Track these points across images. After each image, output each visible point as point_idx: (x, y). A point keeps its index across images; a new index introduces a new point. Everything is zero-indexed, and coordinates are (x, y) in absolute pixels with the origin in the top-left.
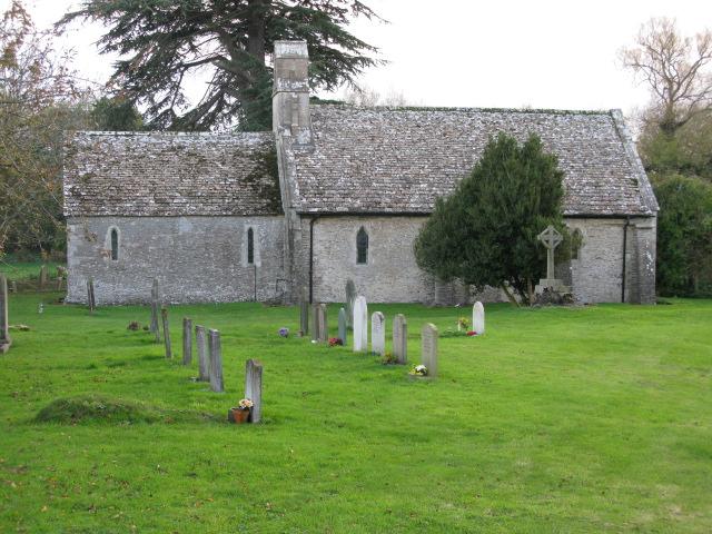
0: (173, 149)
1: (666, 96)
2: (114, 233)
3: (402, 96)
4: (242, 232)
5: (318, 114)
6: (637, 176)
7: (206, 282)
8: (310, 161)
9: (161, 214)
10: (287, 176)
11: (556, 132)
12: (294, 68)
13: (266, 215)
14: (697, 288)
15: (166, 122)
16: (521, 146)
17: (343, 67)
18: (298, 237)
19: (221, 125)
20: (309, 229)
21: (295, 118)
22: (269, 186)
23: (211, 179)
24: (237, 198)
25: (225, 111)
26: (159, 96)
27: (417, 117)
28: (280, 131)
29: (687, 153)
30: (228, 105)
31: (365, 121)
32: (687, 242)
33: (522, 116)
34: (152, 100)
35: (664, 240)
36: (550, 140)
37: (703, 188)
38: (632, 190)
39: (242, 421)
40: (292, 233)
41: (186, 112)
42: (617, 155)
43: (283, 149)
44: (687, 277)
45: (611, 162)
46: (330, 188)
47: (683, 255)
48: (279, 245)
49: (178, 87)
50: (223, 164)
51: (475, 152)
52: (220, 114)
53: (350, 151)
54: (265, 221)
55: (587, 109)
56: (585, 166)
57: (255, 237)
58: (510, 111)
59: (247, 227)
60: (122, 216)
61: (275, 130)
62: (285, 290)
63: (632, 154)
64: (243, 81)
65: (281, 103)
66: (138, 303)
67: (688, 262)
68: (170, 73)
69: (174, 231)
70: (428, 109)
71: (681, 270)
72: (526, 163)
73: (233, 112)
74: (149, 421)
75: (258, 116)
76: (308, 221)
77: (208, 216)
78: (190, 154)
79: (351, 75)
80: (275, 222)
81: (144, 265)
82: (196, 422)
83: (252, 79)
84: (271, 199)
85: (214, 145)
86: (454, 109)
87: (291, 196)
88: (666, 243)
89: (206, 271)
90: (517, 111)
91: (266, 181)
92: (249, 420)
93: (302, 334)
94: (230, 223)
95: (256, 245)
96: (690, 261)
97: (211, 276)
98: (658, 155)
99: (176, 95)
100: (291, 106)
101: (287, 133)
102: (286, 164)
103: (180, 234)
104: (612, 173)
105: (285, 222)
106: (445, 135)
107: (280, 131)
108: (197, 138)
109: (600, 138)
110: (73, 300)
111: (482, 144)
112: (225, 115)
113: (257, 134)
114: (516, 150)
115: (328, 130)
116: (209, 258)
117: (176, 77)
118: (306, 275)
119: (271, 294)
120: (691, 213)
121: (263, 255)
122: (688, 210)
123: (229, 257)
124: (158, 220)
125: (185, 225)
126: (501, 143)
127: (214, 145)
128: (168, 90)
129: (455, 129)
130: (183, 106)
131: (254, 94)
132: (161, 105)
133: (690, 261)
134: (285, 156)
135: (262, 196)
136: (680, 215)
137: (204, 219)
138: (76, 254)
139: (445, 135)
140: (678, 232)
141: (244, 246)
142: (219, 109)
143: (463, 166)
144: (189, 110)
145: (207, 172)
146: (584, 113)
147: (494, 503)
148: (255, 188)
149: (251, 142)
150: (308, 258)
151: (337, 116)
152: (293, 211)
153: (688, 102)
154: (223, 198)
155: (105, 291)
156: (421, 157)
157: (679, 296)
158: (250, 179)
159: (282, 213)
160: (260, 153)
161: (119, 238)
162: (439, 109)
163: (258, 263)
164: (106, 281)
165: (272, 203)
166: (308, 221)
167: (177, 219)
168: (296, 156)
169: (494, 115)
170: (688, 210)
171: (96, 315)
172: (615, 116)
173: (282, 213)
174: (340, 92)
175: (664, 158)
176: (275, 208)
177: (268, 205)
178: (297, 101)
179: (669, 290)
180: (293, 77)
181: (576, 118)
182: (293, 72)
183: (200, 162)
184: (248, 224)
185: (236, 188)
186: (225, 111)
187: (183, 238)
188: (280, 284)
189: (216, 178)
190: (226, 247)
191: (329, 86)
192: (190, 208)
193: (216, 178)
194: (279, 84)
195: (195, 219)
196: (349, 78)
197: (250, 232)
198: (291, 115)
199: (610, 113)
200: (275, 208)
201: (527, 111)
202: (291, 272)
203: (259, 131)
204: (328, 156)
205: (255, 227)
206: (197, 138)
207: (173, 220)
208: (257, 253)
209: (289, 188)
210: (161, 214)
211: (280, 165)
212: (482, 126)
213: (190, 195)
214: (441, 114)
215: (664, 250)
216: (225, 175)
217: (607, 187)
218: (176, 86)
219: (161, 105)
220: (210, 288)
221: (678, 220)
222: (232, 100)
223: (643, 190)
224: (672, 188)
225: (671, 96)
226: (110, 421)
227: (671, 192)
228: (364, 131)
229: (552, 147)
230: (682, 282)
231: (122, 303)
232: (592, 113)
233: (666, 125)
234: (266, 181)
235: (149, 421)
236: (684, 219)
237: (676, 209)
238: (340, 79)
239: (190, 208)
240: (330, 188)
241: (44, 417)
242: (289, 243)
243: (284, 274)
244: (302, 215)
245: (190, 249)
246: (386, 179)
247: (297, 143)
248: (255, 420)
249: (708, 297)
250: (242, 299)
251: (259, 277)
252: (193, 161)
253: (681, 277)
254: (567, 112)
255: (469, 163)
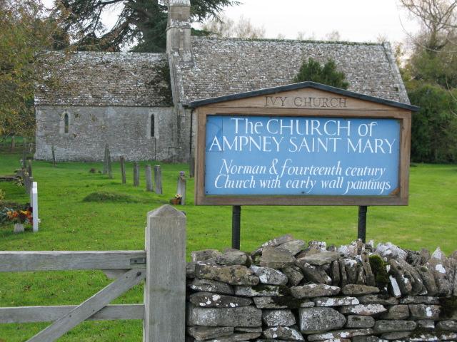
0: (103, 63)
1: (431, 27)
2: (66, 116)
3: (249, 23)
4: (148, 117)
5: (196, 43)
6: (398, 86)
7: (124, 148)
8: (191, 72)
9: (96, 104)
10: (176, 81)
11: (348, 57)
12: (181, 13)
13: (163, 107)
14: (436, 158)
15: (89, 43)
16: (323, 65)
17: (210, 6)
18: (183, 121)
19: (126, 43)
20: (190, 116)
21: (182, 45)
22: (384, 243)
23: (127, 83)
24: (145, 95)
25: (129, 34)
26: (86, 23)
27: (259, 46)
28: (172, 53)
29: (444, 67)
30: (131, 30)
31: (226, 47)
32: (431, 128)
33: (326, 46)
34: (80, 26)
35: (416, 126)
36: (343, 62)
37: (442, 93)
38: (394, 94)
39: (177, 204)
40: (179, 118)
41: (103, 34)
42: (386, 71)
43: (174, 64)
44: (430, 150)
45: (382, 76)
46: (203, 90)
47: (428, 136)
48: (171, 125)
49: (98, 18)
50: (135, 73)
51: (295, 68)
52: (126, 36)
53: (216, 66)
54: (162, 110)
55: (368, 42)
56: (366, 78)
57: (156, 120)
58: (319, 42)
59: (150, 114)
60: (71, 105)
61: (168, 51)
62: (174, 154)
63: (396, 71)
64: (143, 15)
65: (172, 34)
66: (81, 161)
67: (431, 141)
68: (92, 8)
69: (104, 115)
70: (266, 40)
71: (427, 146)
72: (325, 78)
73: (134, 35)
74: (136, 202)
75: (156, 41)
76: (189, 111)
77: (127, 106)
78: (114, 67)
79: (215, 11)
80: (168, 111)
81: (85, 137)
82: (155, 203)
83: (150, 14)
84: (166, 97)
85: (129, 61)
86: (283, 41)
87: (179, 95)
88: (417, 128)
89: (124, 141)
90: (323, 42)
91: (163, 84)
92: (180, 203)
93: (191, 176)
94: (140, 111)
95: (156, 125)
96: (432, 140)
97: (128, 144)
98: (423, 68)
99: (97, 23)
100: (179, 37)
101: (176, 54)
102: (176, 74)
103: (109, 117)
104: (382, 83)
105: (175, 111)
106: (276, 57)
107: (172, 53)
108: (118, 56)
109: (376, 60)
110: (40, 158)
111: (300, 64)
112: (129, 36)
113: (157, 54)
114: (319, 70)
115: (202, 53)
116: (126, 133)
117: (97, 11)
118: (188, 145)
119: (165, 156)
120: (434, 109)
121: (160, 132)
122: (432, 107)
123: (139, 133)
124: (94, 108)
125: (111, 112)
126: (310, 65)
127: (129, 61)
128: (91, 20)
129: (283, 53)
130: (101, 31)
131: (151, 25)
132: (86, 30)
133: (432, 140)
134: (175, 69)
135: (160, 94)
136: (427, 110)
137: (124, 108)
138: (42, 129)
139: (276, 57)
140: (426, 121)
141: (149, 126)
142: (125, 33)
143: (288, 77)
144: (105, 33)
145: (125, 78)
146: (366, 44)
147: (321, 316)
148: (156, 89)
149: (153, 59)
150: (189, 134)
151: (208, 44)
152: (180, 104)
153: (445, 31)
154: (136, 95)
155: (62, 153)
156: (261, 71)
157: (425, 162)
158: (152, 83)
159: (172, 105)
160: (158, 67)
161: (69, 118)
162: (273, 40)
163: (157, 136)
164: (61, 146)
165: (166, 99)
166: (189, 111)
167: (107, 108)
168: (182, 69)
169: (308, 45)
170: (432, 107)
171: (58, 167)
172: (386, 47)
173: (172, 105)
174: (207, 22)
175: (427, 71)
176: (168, 102)
177: (164, 100)
178: (183, 34)
179: (419, 158)
180: (181, 18)
181: (361, 47)
182: (180, 15)
183: (119, 72)
184: (151, 112)
185: (144, 89)
186: (129, 34)
187: (110, 120)
188: (171, 150)
189: (131, 82)
190: (137, 126)
191: (200, 19)
192: (115, 101)
193: (134, 83)
194: (171, 22)
195: (118, 108)
196: (214, 14)
197: (153, 117)
198: (179, 43)
199: (383, 45)
200: (168, 102)
201: (329, 43)
202: (178, 142)
203: (158, 52)
204: (202, 69)
205: (156, 114)
206: (118, 56)
207: (104, 108)
208: (156, 131)
209: (178, 89)
210: (96, 104)
211: (171, 74)
212: (300, 52)
213: (115, 93)
214: (274, 43)
215: (416, 133)
216: (137, 81)
217: (378, 92)
218: (97, 17)
219: (86, 30)
220: (127, 152)
221: (426, 113)
222: (133, 27)
223: (401, 94)
224: (422, 92)
225: (435, 28)
226: (119, 202)
227: (421, 95)
228: (225, 54)
229: (345, 66)
230: (427, 154)
231: (71, 161)
232: (371, 44)
233: (430, 47)
234: (163, 84)
235: (136, 202)
236: (429, 113)
237: (425, 106)
238: (208, 14)
239: (115, 101)
240: (203, 90)
241: (87, 200)
242: (177, 124)
243: (173, 144)
244: (186, 107)
245: (115, 127)
246: (239, 85)
247: (182, 61)
248: (183, 203)
249: (449, 160)
250: (147, 159)
251: (158, 145)
252: (116, 71)
253: (425, 150)
254: (355, 43)
255: (291, 76)
